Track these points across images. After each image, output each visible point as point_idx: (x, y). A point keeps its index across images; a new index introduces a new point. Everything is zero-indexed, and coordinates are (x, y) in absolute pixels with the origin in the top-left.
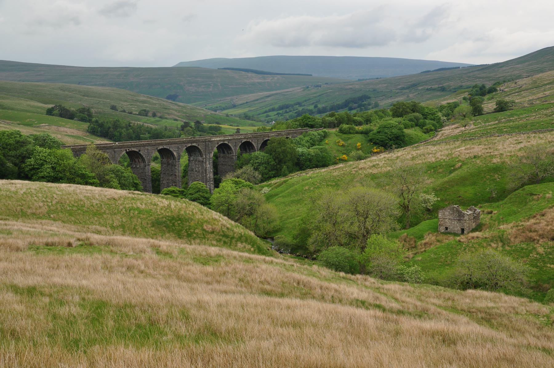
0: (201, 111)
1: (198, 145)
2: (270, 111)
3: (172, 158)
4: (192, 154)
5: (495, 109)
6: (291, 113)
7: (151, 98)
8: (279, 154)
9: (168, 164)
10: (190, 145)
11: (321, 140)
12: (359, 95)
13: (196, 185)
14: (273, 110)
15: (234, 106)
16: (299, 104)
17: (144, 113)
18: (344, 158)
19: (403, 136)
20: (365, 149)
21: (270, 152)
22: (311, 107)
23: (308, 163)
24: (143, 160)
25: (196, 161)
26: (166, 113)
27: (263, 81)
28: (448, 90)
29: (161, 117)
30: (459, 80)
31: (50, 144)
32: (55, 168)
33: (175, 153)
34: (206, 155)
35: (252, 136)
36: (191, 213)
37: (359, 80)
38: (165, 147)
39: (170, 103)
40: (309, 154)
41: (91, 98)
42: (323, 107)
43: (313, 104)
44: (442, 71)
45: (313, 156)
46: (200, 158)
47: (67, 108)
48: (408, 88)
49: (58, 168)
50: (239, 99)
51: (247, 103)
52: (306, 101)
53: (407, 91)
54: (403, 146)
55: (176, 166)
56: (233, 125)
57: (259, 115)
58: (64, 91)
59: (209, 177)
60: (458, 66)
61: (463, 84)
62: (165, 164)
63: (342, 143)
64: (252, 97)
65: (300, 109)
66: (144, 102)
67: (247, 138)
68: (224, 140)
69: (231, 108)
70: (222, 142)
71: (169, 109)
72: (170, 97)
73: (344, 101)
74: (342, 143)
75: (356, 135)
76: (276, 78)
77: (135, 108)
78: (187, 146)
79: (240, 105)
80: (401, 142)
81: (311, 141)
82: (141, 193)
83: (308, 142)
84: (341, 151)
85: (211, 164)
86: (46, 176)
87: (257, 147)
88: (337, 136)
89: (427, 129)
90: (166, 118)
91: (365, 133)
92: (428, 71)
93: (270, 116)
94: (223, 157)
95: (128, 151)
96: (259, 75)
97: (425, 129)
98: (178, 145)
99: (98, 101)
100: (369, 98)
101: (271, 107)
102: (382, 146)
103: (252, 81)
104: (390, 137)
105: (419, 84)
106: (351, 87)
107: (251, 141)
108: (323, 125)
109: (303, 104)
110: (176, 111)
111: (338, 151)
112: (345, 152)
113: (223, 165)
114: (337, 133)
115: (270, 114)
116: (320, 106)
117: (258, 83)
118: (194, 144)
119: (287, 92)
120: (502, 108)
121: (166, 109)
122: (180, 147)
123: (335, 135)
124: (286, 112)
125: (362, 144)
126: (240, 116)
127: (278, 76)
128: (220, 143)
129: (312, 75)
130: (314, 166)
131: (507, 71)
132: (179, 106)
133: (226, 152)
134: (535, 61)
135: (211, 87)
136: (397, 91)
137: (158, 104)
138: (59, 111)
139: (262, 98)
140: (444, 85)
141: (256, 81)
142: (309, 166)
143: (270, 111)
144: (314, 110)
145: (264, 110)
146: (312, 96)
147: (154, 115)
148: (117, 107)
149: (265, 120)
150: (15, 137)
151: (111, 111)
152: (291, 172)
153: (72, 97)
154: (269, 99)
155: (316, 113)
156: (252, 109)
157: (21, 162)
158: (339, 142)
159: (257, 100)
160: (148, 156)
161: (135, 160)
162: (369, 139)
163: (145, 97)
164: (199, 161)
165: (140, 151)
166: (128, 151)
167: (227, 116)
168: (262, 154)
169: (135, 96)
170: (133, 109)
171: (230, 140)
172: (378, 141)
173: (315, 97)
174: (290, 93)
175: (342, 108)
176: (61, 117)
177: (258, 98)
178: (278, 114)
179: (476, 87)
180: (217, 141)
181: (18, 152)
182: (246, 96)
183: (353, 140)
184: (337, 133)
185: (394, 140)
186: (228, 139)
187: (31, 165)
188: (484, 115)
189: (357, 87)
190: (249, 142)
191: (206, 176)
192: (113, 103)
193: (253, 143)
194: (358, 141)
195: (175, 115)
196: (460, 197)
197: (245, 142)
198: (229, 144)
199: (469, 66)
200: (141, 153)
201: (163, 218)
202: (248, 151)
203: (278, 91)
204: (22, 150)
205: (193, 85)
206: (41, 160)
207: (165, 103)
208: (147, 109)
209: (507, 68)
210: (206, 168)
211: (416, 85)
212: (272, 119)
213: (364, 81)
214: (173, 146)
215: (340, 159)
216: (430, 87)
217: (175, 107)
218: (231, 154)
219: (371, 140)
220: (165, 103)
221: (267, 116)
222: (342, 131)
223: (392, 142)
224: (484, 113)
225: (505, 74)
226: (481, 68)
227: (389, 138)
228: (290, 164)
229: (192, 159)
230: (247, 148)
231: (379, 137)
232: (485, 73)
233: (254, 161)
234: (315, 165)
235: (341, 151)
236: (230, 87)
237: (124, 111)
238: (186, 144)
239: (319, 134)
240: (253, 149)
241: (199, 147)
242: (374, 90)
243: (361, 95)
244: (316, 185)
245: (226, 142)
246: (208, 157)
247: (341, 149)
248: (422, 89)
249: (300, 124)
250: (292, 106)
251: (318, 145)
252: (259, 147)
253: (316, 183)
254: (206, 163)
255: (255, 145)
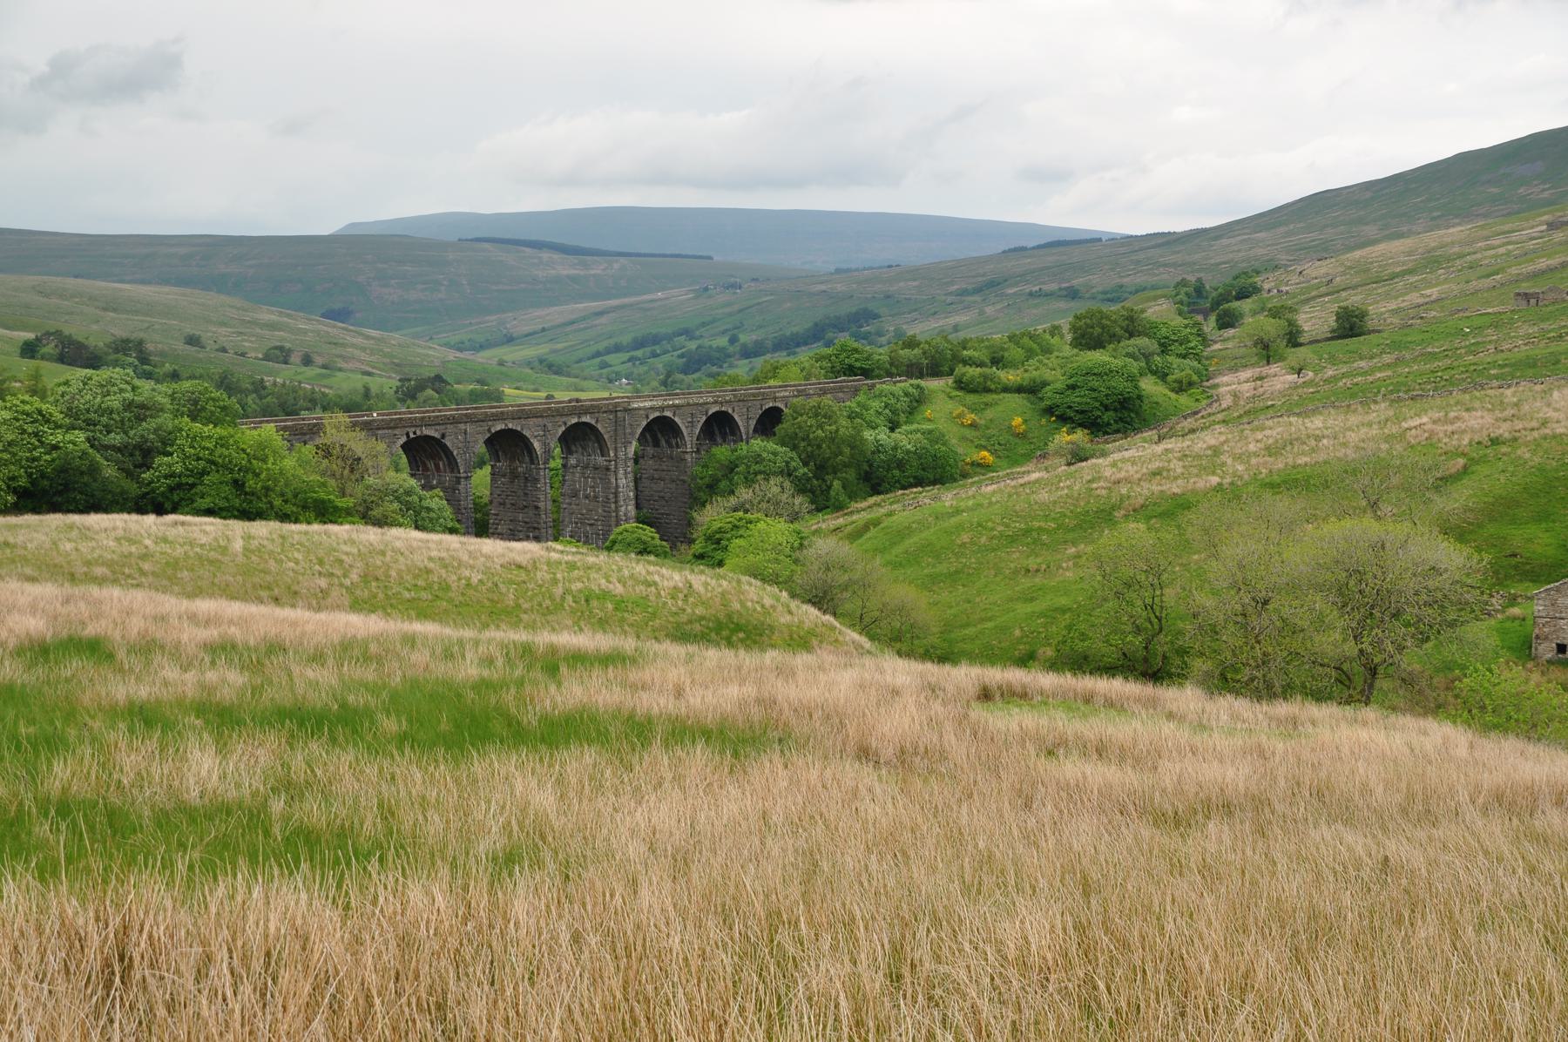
0: (431, 352)
1: (597, 422)
2: (608, 351)
3: (527, 459)
4: (574, 448)
5: (1333, 331)
6: (666, 358)
7: (288, 316)
8: (819, 447)
9: (514, 476)
10: (574, 420)
11: (911, 412)
12: (846, 309)
13: (633, 532)
14: (617, 349)
15: (510, 340)
16: (687, 333)
17: (281, 355)
18: (984, 458)
19: (1140, 397)
20: (1036, 434)
21: (791, 442)
22: (723, 341)
23: (896, 472)
24: (450, 463)
25: (586, 467)
26: (338, 356)
27: (582, 273)
28: (1087, 295)
29: (324, 367)
30: (1112, 270)
31: (211, 412)
32: (243, 484)
33: (536, 445)
34: (616, 449)
35: (735, 396)
36: (759, 609)
37: (838, 271)
38: (510, 426)
39: (343, 328)
40: (895, 448)
41: (125, 316)
42: (756, 342)
43: (724, 332)
44: (1061, 249)
45: (908, 452)
46: (600, 460)
47: (80, 339)
48: (978, 291)
49: (251, 483)
50: (524, 321)
51: (544, 330)
52: (704, 324)
53: (977, 298)
54: (1136, 426)
55: (537, 480)
56: (525, 387)
57: (580, 361)
58: (47, 296)
59: (625, 515)
60: (1098, 237)
61: (1125, 280)
62: (504, 476)
63: (970, 417)
64: (556, 314)
65: (693, 345)
66: (272, 326)
67: (721, 403)
68: (662, 409)
69: (503, 344)
70: (657, 414)
71: (344, 345)
72: (332, 315)
73: (810, 324)
74: (970, 417)
75: (1003, 395)
76: (616, 266)
77: (251, 342)
78: (569, 424)
79: (526, 336)
80: (1133, 415)
81: (887, 411)
82: (574, 550)
83: (880, 413)
84: (972, 441)
85: (631, 476)
86: (221, 509)
87: (747, 428)
88: (951, 397)
89: (1180, 382)
90: (340, 370)
91: (1031, 390)
92: (1023, 249)
93: (610, 366)
94: (654, 456)
95: (412, 436)
96: (570, 257)
97: (1175, 381)
98: (545, 421)
99: (146, 325)
100: (876, 316)
101: (612, 342)
102: (1082, 425)
103: (553, 272)
104: (1106, 402)
105: (1006, 281)
106: (823, 287)
107: (730, 411)
108: (894, 370)
109: (698, 333)
110: (364, 349)
111: (964, 439)
112: (983, 443)
113: (653, 479)
114: (948, 390)
115: (609, 358)
116: (744, 338)
117: (568, 277)
118: (586, 419)
119: (652, 301)
120: (1351, 329)
121: (335, 344)
122: (550, 426)
123: (943, 396)
124: (655, 355)
125: (1025, 421)
126: (529, 364)
127: (622, 260)
128: (651, 417)
129: (710, 258)
130: (912, 480)
131: (1236, 248)
132: (368, 337)
133: (663, 443)
134: (1302, 225)
135: (443, 288)
136: (949, 299)
137: (312, 331)
138: (56, 346)
139: (584, 319)
140: (1075, 282)
141: (565, 272)
142: (898, 481)
143: (608, 351)
144: (731, 349)
145: (594, 349)
146: (720, 311)
147: (307, 361)
148: (203, 340)
149: (601, 376)
150: (122, 390)
151: (188, 347)
152: (853, 497)
153: (72, 313)
154: (604, 320)
155: (737, 356)
156: (559, 346)
157: (140, 466)
158: (959, 416)
159: (572, 323)
160: (465, 453)
161: (424, 464)
162: (1043, 405)
163: (272, 313)
164: (596, 469)
165: (443, 436)
166: (412, 436)
167: (501, 363)
168: (771, 445)
169: (246, 311)
170: (246, 344)
171: (677, 407)
172: (1071, 413)
173: (730, 314)
174: (659, 303)
175: (806, 344)
176: (63, 363)
177: (574, 317)
178: (630, 360)
179: (1185, 286)
180: (645, 409)
181: (135, 435)
182: (538, 312)
183: (1000, 408)
184: (948, 390)
185: (1115, 410)
186: (673, 406)
187: (172, 475)
188: (1301, 349)
189: (840, 287)
190: (725, 414)
191: (617, 511)
192: (189, 329)
193: (736, 417)
194: (1015, 413)
195: (362, 362)
196: (1515, 556)
197: (717, 412)
198: (676, 419)
199: (1111, 237)
200: (448, 444)
201: (690, 622)
202: (719, 440)
203: (627, 300)
204: (146, 429)
205: (393, 282)
206: (199, 459)
207: (330, 330)
208: (287, 345)
209: (1233, 241)
210: (617, 486)
211: (999, 284)
212: (617, 373)
213: (856, 274)
214: (532, 422)
215: (973, 464)
216: (1037, 288)
217: (359, 340)
218: (678, 447)
219: (1049, 411)
220: (330, 330)
221: (604, 365)
222: (961, 385)
223: (1111, 413)
224: (1301, 340)
225: (1231, 256)
226: (1164, 240)
227: (1102, 404)
228: (851, 475)
229: (573, 461)
230: (717, 432)
231: (1074, 399)
232: (1178, 252)
233: (748, 467)
234: (915, 477)
235: (972, 441)
236: (494, 287)
237: (224, 350)
238: (564, 419)
239: (907, 394)
240: (733, 434)
241: (599, 427)
242: (888, 297)
243: (854, 310)
244: (993, 529)
245: (668, 414)
246: (621, 454)
247: (969, 433)
248: (1015, 294)
249: (833, 367)
250: (669, 338)
251: (906, 423)
252: (752, 427)
253: (990, 524)
254: (616, 473)
255: (740, 423)
